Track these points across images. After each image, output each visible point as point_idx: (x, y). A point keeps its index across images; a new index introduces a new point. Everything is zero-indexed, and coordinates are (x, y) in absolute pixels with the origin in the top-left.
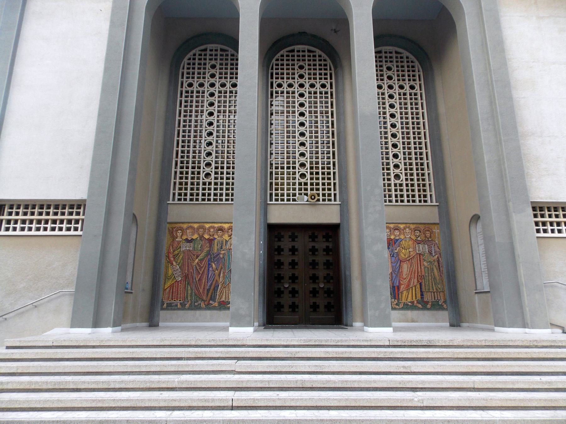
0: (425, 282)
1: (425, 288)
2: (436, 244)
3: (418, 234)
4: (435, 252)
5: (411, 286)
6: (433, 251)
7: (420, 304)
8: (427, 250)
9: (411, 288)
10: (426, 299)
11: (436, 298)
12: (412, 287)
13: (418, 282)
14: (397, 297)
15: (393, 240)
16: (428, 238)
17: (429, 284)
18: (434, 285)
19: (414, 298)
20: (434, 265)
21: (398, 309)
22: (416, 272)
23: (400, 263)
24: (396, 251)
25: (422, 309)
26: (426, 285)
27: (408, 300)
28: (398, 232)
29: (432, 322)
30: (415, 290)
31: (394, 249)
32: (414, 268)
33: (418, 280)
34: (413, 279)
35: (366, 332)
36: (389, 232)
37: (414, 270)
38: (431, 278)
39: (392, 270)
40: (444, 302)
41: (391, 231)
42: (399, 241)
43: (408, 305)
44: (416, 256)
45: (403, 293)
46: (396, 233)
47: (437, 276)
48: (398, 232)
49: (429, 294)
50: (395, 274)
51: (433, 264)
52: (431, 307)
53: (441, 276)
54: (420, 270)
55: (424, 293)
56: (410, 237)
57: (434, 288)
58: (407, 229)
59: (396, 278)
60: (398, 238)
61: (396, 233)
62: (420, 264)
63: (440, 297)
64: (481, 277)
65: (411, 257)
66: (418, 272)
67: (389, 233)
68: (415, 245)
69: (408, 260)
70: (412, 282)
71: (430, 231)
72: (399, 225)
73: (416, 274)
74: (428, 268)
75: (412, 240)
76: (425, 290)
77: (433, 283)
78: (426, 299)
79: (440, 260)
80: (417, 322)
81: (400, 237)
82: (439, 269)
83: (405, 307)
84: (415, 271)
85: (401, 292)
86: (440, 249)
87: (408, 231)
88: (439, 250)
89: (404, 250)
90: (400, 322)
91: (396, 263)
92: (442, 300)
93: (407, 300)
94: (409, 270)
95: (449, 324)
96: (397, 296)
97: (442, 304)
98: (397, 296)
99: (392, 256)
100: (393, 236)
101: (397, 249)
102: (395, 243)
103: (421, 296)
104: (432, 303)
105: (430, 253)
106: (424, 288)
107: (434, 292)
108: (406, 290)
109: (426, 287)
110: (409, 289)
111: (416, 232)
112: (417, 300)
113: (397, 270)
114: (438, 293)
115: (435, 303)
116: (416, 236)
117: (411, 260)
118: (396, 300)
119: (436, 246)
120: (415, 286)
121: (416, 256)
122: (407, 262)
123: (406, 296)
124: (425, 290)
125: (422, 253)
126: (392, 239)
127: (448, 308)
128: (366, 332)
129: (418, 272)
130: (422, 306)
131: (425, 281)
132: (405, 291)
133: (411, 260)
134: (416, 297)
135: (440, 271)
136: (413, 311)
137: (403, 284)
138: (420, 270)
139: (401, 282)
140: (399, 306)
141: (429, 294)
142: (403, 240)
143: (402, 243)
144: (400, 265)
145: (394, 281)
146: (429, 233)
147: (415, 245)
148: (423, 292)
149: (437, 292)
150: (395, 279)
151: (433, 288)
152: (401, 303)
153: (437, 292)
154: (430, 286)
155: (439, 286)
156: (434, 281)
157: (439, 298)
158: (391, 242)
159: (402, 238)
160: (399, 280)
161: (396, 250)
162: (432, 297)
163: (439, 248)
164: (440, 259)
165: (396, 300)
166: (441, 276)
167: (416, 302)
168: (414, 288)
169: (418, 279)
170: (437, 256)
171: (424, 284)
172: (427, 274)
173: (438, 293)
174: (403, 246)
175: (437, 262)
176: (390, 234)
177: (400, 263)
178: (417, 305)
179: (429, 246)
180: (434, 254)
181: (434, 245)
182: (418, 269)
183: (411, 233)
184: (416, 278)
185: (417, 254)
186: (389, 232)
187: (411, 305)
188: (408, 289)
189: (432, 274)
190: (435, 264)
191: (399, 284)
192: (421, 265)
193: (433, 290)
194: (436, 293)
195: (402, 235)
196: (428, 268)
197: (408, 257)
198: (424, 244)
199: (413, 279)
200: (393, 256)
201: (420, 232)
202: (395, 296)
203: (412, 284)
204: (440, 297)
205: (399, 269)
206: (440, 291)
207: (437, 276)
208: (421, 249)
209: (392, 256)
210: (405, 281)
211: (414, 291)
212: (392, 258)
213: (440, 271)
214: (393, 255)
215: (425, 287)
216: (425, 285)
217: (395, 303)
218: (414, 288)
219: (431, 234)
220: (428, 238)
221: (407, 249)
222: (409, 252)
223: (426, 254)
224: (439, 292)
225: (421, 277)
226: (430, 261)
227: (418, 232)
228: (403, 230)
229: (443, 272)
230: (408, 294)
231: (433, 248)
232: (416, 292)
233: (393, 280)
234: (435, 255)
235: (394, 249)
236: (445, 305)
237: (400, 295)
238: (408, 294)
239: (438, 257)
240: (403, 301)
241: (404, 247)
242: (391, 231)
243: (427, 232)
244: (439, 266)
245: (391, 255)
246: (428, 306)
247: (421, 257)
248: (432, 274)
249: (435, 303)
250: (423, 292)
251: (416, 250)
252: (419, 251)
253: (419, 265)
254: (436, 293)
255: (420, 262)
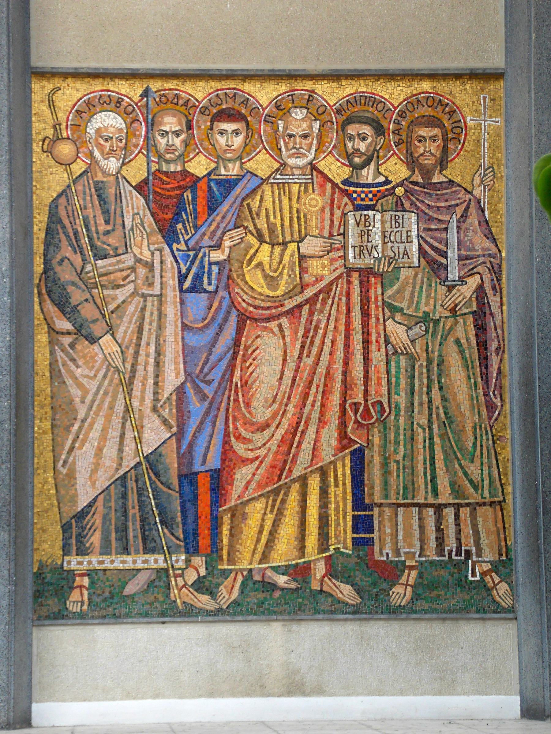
0: (384, 447)
1: (386, 484)
2: (473, 210)
3: (362, 146)
4: (461, 258)
5: (297, 473)
6: (453, 254)
7: (348, 580)
8: (415, 248)
9: (296, 486)
10: (387, 549)
11: (451, 544)
12: (303, 480)
13: (343, 448)
14: (204, 542)
15: (203, 185)
16: (427, 173)
17: (411, 456)
18: (440, 464)
19: (312, 541)
20: (451, 339)
21: (209, 613)
22: (338, 386)
23: (240, 331)
24: (217, 256)
25: (356, 611)
26: (393, 466)
27: (274, 555)
28: (236, 132)
29: (415, 691)
30: (324, 492)
31: (206, 241)
32: (325, 358)
33: (343, 435)
34: (312, 430)
35: (38, 727)
36: (177, 134)
37: (321, 370)
38: (424, 421)
39: (188, 374)
40: (496, 567)
41: (190, 127)
42: (237, 190)
43: (273, 587)
44: (340, 287)
45: (245, 517)
46: (222, 140)
47: (465, 408)
48: (236, 132)
49: (408, 518)
50: (204, 397)
51: (445, 338)
52: (416, 596)
53: (491, 407)
54: (358, 372)
55: (376, 510)
56: (314, 167)
57: (443, 483)
58: (299, 114)
59: (208, 428)
60: (233, 170)
61: (222, 140)
62: (366, 334)
63: (476, 533)
64: (159, 450)
65: (309, 293)
66: (344, 382)
67: (177, 141)
68: (338, 213)
69: (290, 312)
70: (308, 446)
71: (439, 124)
72: (248, 87)
73: (336, 398)
74: (412, 359)
75: (322, 186)
76: (386, 497)
77: (438, 449)
78: (387, 549)
79: (495, 308)
80: (319, 691)
81: (248, 165)
82: (484, 360)
83: (254, 598)
84: (328, 374)
85: (233, 511)
86: (494, 241)
87: (297, 129)
88: (488, 244)
89: (266, 248)
90: (211, 694)
91: (211, 332)
92: (489, 555)
93: (264, 558)
94: (289, 374)
95: (517, 699)
96: (205, 531)
97: (482, 583)
98: (205, 531)
99: (187, 284)
100: (201, 158)
101: (227, 243)
102: (212, 208)
103: (355, 529)
104: (420, 576)
105: (431, 262)
106: (378, 483)
107: (439, 508)
108: (266, 496)
109: (393, 480)
110: (288, 487)
111: (352, 130)
112: (328, 559)
113: (216, 375)
114: (465, 512)
115: (444, 574)
116: (349, 157)
117: (311, 313)
118: (199, 561)
119: (473, 220)
120: (323, 472)
121: (340, 287)
122: (284, 321)
123: (261, 532)
124: (386, 497)
125: (383, 267)
126: (198, 179)
127: (520, 608)
128: (38, 727)
129: (346, 386)
130: (359, 591)
131: (385, 438)
132: (259, 505)
133: (311, 313)
134: (324, 536)
135: (486, 378)
136: (295, 627)
137: (246, 461)
138: (358, 372)
139: (240, 448)
140: (212, 594)
141: (408, 518)
142: (267, 188)
143: (255, 204)
144: (237, 343)
145: (191, 445)
146: (433, 139)
147: (338, 213)
148: (370, 507)
149: (457, 507)
150: (199, 429)
151: (434, 479)
152: (225, 574)
153: (457, 507)
154: (420, 467)
155: (474, 470)
156: (442, 437)
157: (469, 544)
158: (188, 195)
159: (263, 171)
160: (227, 434)
161: (218, 246)
162: (422, 541)
163: (490, 236)
164: (494, 300)
165: (199, 561)
166: (491, 407)
167: (320, 569)
168: (314, 483)
169: (343, 425)
170: (473, 282)
171: (377, 459)
172: (402, 399)
173: (465, 512)
174: (262, 224)
175: (470, 320)
176: (186, 144)
177: (240, 331)
178: (329, 585)
179: (431, 219)
180: (453, 274)
181: (464, 216)
182: (346, 363)
183: (320, 136)
184: (335, 423)
185: (350, 271)
186: (177, 134)
187: (293, 585)
188: (276, 491)
189: (435, 393)
190: (460, 332)
191: (223, 461)
192: (366, 343)
193: (435, 493)
194: (449, 513)
195: (263, 156)
196: (412, 359)
197: (289, 295)
198: (399, 206)
199: (312, 430)
200: (196, 288)
201: (379, 130)
202: (196, 534)
203: (305, 456)
204: (476, 533)
205: (231, 367)
206: (474, 497)
207: (465, 408)
208: (377, 240)
209: (187, 284)
210: (259, 438)
211: (313, 501)
212: (190, 296)
213: (486, 378)
214: (198, 277)
215: (386, 473)
216: (385, 465)
217: (191, 577)
218: (314, 483)
219: (446, 140)
220: (427, 173)
221: (285, 244)
222: (302, 258)
223: (404, 273)
224: (474, 507)
225: (367, 414)
226: (426, 318)
227: (367, 130)
228: (270, 120)
229: (506, 382)
230: (276, 524)
231: (453, 237)
232: (324, 504)
233: (188, 437)
234: (462, 280)
235: (206, 241)
236: (503, 587)
237: (225, 530)
238: (276, 524)
239: (480, 288)
240: (244, 565)
241: (272, 230)
242: (190, 127)
243: (423, 132)
244: (482, 345)
245: (182, 278)
246: (398, 589)
247: (375, 291)
248: (435, 393)
249: (444, 574)
250: (370, 507)
251: (344, 247)
252: (361, 250)
253: (357, 338)
254: (449, 513)
255: (365, 324)
